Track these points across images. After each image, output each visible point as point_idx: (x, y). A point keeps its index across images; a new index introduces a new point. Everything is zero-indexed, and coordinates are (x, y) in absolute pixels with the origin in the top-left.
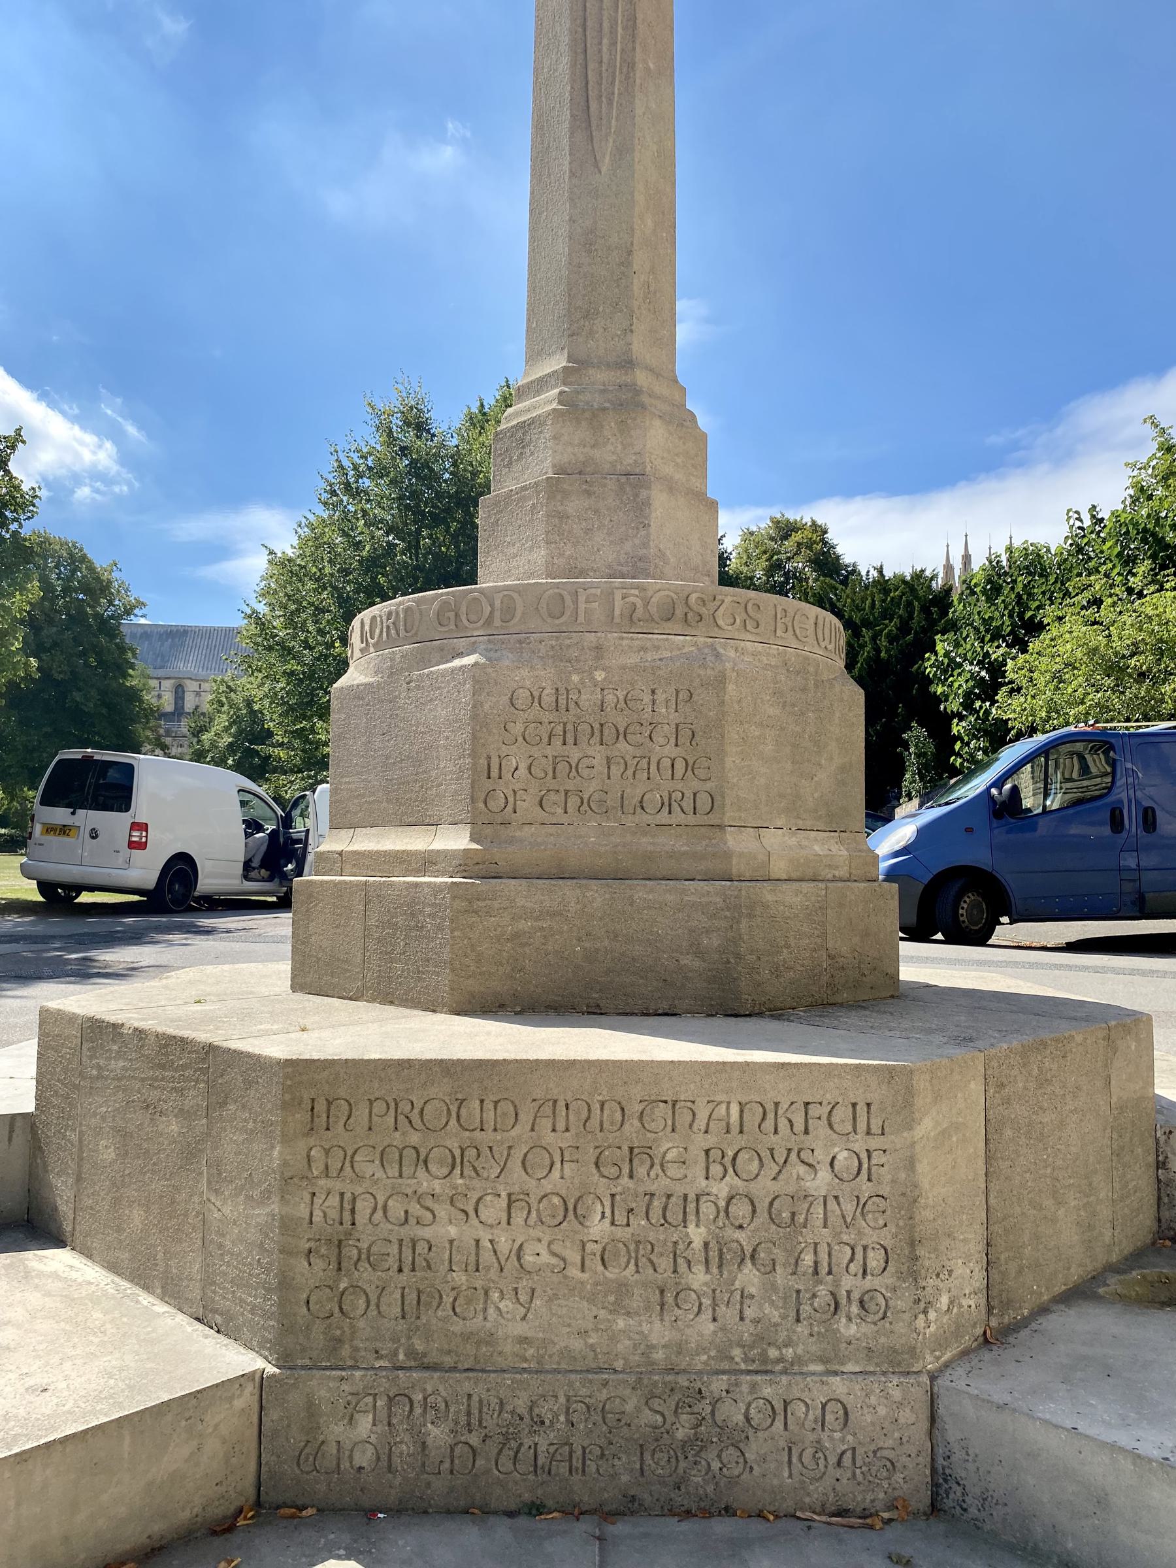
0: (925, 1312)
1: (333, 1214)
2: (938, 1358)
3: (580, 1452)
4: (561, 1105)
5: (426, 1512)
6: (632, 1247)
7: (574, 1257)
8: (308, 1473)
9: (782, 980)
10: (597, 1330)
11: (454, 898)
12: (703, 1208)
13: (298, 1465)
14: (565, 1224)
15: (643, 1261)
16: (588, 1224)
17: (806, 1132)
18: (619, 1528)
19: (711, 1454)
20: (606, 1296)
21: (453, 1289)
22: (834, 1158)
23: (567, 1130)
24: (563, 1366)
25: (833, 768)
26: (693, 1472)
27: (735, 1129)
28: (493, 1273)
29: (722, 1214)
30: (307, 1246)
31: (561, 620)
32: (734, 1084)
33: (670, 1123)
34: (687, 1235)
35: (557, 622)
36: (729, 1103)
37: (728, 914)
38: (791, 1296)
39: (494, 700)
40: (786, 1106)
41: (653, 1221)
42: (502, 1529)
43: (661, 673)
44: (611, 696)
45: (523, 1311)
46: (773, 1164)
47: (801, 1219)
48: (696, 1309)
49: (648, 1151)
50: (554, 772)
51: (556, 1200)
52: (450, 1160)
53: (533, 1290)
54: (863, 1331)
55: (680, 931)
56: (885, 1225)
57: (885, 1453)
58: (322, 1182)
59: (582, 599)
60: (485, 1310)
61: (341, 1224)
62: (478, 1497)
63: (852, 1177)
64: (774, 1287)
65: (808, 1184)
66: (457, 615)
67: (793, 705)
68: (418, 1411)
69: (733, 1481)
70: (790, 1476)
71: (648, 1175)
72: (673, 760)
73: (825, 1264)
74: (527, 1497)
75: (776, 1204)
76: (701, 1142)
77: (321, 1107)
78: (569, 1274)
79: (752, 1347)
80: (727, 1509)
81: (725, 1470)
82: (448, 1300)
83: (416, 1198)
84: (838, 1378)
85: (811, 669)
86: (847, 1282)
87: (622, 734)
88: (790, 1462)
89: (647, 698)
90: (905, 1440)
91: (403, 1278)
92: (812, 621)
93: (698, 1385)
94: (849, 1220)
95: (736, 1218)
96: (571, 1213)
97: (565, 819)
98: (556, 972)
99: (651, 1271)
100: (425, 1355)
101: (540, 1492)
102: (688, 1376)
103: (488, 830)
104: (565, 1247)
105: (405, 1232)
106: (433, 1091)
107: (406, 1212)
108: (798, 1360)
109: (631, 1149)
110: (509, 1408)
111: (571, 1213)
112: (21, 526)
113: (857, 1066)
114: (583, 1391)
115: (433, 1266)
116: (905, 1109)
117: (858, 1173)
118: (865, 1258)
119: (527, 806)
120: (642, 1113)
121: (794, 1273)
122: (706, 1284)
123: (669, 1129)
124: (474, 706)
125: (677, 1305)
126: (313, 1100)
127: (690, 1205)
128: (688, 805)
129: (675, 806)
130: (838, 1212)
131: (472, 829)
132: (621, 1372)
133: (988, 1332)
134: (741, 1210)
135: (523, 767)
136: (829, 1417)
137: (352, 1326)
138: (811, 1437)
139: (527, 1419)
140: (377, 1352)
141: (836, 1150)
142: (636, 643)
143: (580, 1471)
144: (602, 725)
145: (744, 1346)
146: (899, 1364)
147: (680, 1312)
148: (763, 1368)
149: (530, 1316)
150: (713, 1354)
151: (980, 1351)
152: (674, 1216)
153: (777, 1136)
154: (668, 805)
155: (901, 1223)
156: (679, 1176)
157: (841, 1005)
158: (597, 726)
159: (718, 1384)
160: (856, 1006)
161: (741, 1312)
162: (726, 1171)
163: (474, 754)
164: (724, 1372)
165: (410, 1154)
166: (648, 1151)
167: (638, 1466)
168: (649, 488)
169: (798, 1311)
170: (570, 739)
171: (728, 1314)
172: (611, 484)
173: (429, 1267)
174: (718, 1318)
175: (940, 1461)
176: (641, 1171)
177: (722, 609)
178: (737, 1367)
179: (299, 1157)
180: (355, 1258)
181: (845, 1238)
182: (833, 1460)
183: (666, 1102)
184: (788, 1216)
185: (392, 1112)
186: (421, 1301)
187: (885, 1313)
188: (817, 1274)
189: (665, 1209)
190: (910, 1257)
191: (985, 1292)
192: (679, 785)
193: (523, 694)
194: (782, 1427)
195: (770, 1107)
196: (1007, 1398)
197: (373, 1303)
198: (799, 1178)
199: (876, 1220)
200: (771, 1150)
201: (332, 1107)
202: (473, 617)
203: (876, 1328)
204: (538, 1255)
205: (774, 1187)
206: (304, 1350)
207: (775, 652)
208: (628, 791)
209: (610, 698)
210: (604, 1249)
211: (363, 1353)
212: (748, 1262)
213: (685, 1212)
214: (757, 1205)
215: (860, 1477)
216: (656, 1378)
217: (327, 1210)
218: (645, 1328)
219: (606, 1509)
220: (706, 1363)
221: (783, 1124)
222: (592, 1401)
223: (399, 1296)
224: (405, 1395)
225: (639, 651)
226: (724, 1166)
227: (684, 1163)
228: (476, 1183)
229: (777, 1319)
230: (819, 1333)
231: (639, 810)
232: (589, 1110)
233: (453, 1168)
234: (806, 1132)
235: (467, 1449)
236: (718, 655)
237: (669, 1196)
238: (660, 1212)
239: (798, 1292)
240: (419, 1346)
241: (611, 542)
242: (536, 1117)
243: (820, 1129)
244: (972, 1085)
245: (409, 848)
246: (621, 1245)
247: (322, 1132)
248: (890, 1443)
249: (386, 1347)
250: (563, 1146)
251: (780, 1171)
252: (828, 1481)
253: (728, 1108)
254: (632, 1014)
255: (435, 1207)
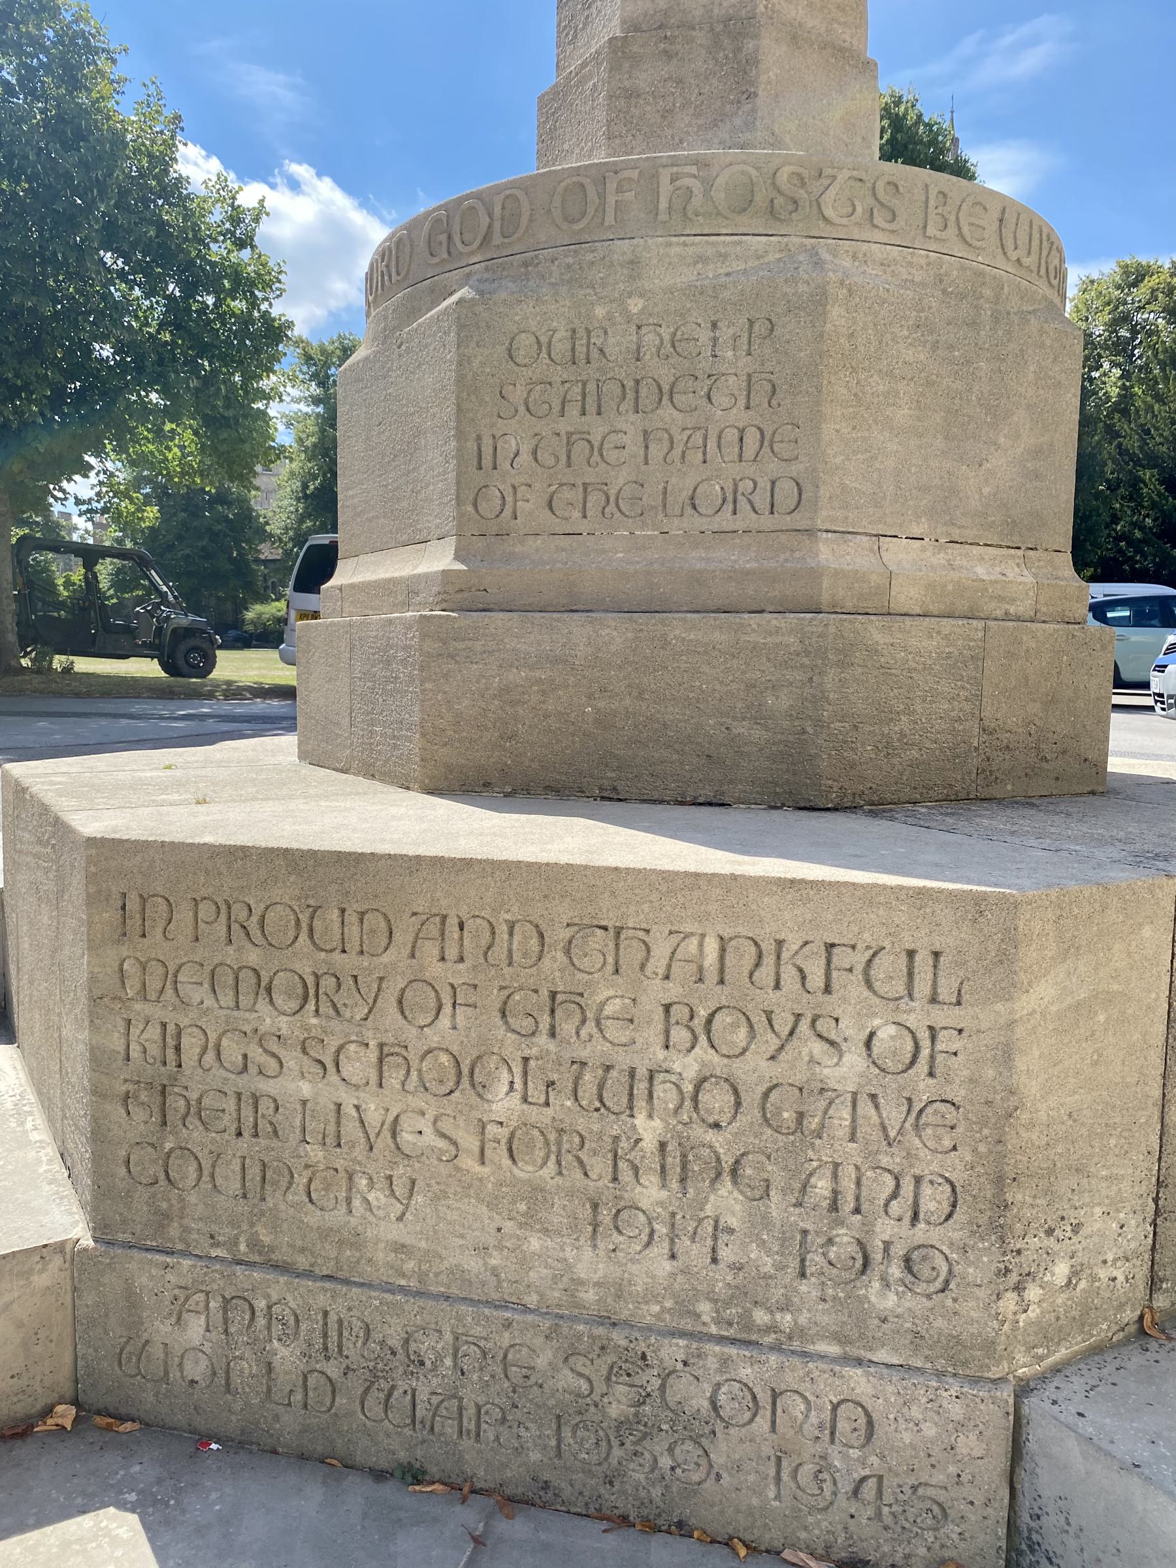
0: (1019, 1288)
1: (154, 1050)
2: (1041, 1358)
3: (472, 1411)
4: (453, 922)
5: (274, 1452)
6: (552, 1137)
7: (470, 1142)
8: (131, 1376)
9: (895, 761)
10: (500, 1248)
11: (424, 636)
12: (658, 1091)
13: (120, 1363)
14: (457, 1094)
15: (567, 1159)
16: (490, 1097)
17: (828, 990)
18: (518, 1528)
19: (659, 1446)
20: (514, 1202)
21: (307, 1166)
22: (872, 1035)
23: (461, 959)
24: (454, 1291)
25: (1020, 450)
26: (632, 1466)
27: (712, 976)
28: (360, 1152)
29: (688, 1103)
30: (124, 1088)
31: (581, 225)
32: (712, 908)
33: (610, 960)
34: (634, 1127)
35: (576, 227)
36: (703, 936)
37: (806, 661)
38: (793, 1238)
39: (487, 352)
40: (795, 947)
41: (584, 1103)
42: (357, 1492)
43: (726, 294)
44: (651, 336)
45: (399, 1208)
46: (770, 1036)
47: (813, 1123)
48: (644, 1237)
49: (578, 999)
50: (569, 457)
51: (444, 1058)
52: (300, 991)
53: (413, 1182)
54: (908, 1305)
55: (734, 686)
56: (955, 1148)
57: (930, 1492)
58: (138, 1006)
59: (611, 186)
60: (349, 1201)
61: (165, 1064)
62: (339, 1443)
63: (901, 1067)
64: (766, 1221)
65: (826, 1071)
66: (450, 237)
67: (951, 347)
68: (261, 1322)
69: (692, 1490)
70: (778, 1497)
71: (578, 1033)
72: (742, 431)
73: (850, 1198)
74: (402, 1455)
75: (773, 1096)
76: (656, 992)
77: (133, 905)
78: (460, 1165)
79: (728, 1304)
80: (680, 1524)
81: (679, 1471)
82: (301, 1180)
83: (256, 1040)
84: (859, 1371)
85: (987, 292)
86: (885, 1229)
87: (667, 394)
88: (778, 1479)
89: (704, 335)
90: (965, 1478)
91: (244, 1144)
92: (996, 215)
93: (642, 1347)
94: (892, 1134)
95: (709, 1112)
96: (465, 1080)
97: (583, 527)
98: (558, 741)
99: (579, 1174)
100: (272, 1249)
101: (419, 1453)
102: (627, 1332)
103: (480, 543)
104: (457, 1127)
105: (242, 1082)
106: (276, 893)
107: (245, 1056)
108: (798, 1332)
109: (553, 995)
110: (377, 1336)
111: (465, 1080)
112: (271, 305)
113: (921, 892)
114: (478, 1331)
115: (280, 1133)
116: (1002, 963)
117: (913, 1063)
118: (916, 1196)
119: (530, 506)
120: (570, 942)
121: (798, 1204)
122: (661, 1203)
123: (610, 968)
124: (460, 364)
125: (617, 1228)
126: (124, 895)
127: (640, 1085)
128: (761, 500)
129: (743, 503)
130: (875, 1119)
131: (458, 543)
132: (532, 1311)
133: (1148, 1317)
134: (717, 1100)
135: (525, 449)
136: (843, 1426)
137: (182, 1200)
138: (810, 1448)
139: (401, 1354)
140: (212, 1237)
141: (877, 1022)
142: (691, 250)
143: (473, 1435)
144: (637, 382)
145: (716, 1301)
146: (965, 1364)
147: (621, 1238)
148: (744, 1336)
149: (408, 1216)
150: (668, 1304)
151: (1125, 1351)
152: (615, 1098)
153: (778, 993)
154: (732, 500)
155: (982, 1148)
156: (624, 1040)
157: (999, 801)
158: (630, 384)
159: (673, 1351)
160: (1028, 802)
161: (714, 1250)
162: (695, 1038)
163: (460, 435)
164: (683, 1334)
165: (247, 977)
166: (578, 999)
167: (553, 1443)
168: (756, 36)
169: (803, 1261)
170: (591, 407)
171: (695, 1253)
172: (701, 37)
173: (275, 1132)
174: (679, 1255)
175: (1025, 1518)
176: (567, 1028)
177: (832, 192)
178: (705, 1329)
179: (109, 971)
180: (183, 1110)
181: (885, 1161)
182: (846, 1487)
183: (605, 928)
184: (795, 1118)
185: (223, 917)
186: (265, 1178)
187: (947, 1282)
188: (837, 1210)
189: (601, 1087)
190: (994, 1204)
191: (1147, 1256)
192: (750, 470)
193: (526, 340)
194: (767, 1427)
195: (768, 947)
196: (1143, 1453)
197: (206, 1173)
198: (812, 1061)
199: (939, 1139)
200: (769, 1015)
201: (148, 906)
202: (468, 237)
203: (929, 1304)
204: (419, 1134)
205: (772, 1071)
206: (124, 1222)
207: (923, 262)
208: (673, 480)
209: (650, 339)
210: (512, 1134)
211: (195, 1236)
212: (727, 1179)
213: (631, 1095)
214: (743, 1095)
215: (888, 1520)
216: (581, 1327)
217: (147, 1045)
218: (570, 1254)
219: (508, 1491)
220: (658, 1316)
221: (789, 975)
222: (489, 1345)
223: (238, 1169)
224: (245, 1299)
225: (695, 263)
226: (693, 1032)
227: (631, 1021)
228: (335, 1024)
229: (768, 1269)
230: (835, 1298)
231: (689, 510)
232: (493, 933)
233: (305, 999)
234: (828, 990)
235: (323, 1380)
236: (818, 264)
237: (608, 1068)
238: (595, 1090)
239: (805, 1232)
240: (266, 1238)
241: (699, 126)
242: (417, 937)
243: (851, 988)
244: (1147, 931)
245: (397, 574)
246: (536, 1133)
247: (137, 939)
248: (939, 1478)
249: (225, 1233)
250: (455, 982)
251: (782, 1047)
252: (836, 1516)
253: (701, 945)
254: (661, 802)
255: (282, 1053)
